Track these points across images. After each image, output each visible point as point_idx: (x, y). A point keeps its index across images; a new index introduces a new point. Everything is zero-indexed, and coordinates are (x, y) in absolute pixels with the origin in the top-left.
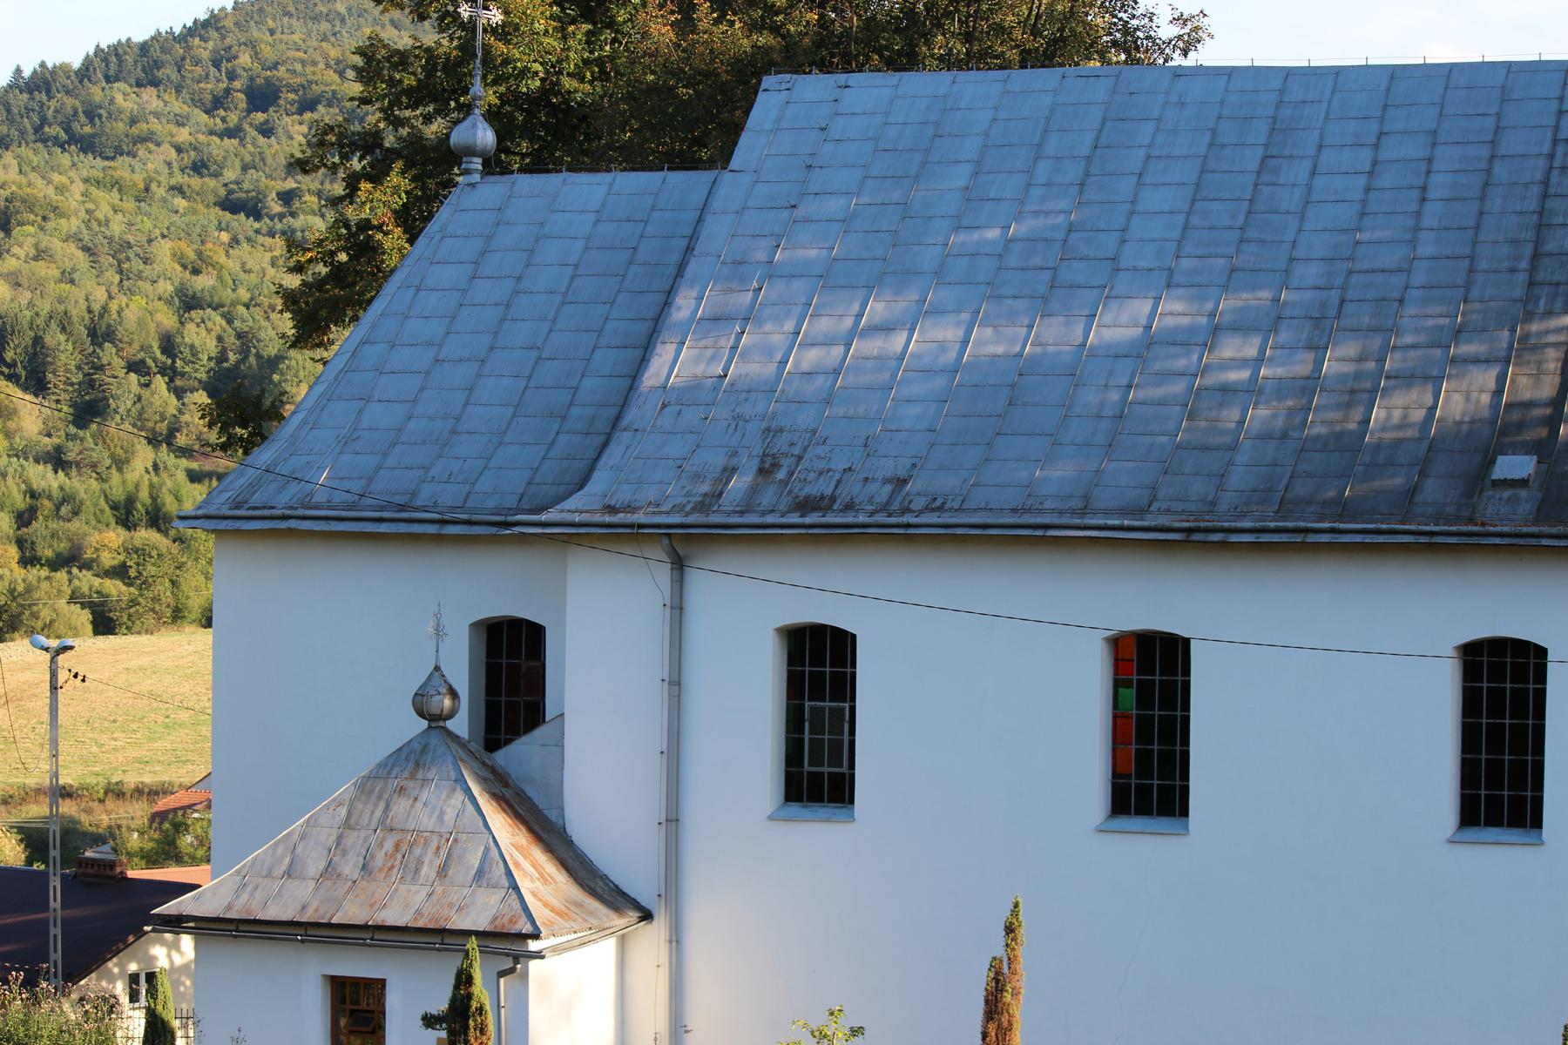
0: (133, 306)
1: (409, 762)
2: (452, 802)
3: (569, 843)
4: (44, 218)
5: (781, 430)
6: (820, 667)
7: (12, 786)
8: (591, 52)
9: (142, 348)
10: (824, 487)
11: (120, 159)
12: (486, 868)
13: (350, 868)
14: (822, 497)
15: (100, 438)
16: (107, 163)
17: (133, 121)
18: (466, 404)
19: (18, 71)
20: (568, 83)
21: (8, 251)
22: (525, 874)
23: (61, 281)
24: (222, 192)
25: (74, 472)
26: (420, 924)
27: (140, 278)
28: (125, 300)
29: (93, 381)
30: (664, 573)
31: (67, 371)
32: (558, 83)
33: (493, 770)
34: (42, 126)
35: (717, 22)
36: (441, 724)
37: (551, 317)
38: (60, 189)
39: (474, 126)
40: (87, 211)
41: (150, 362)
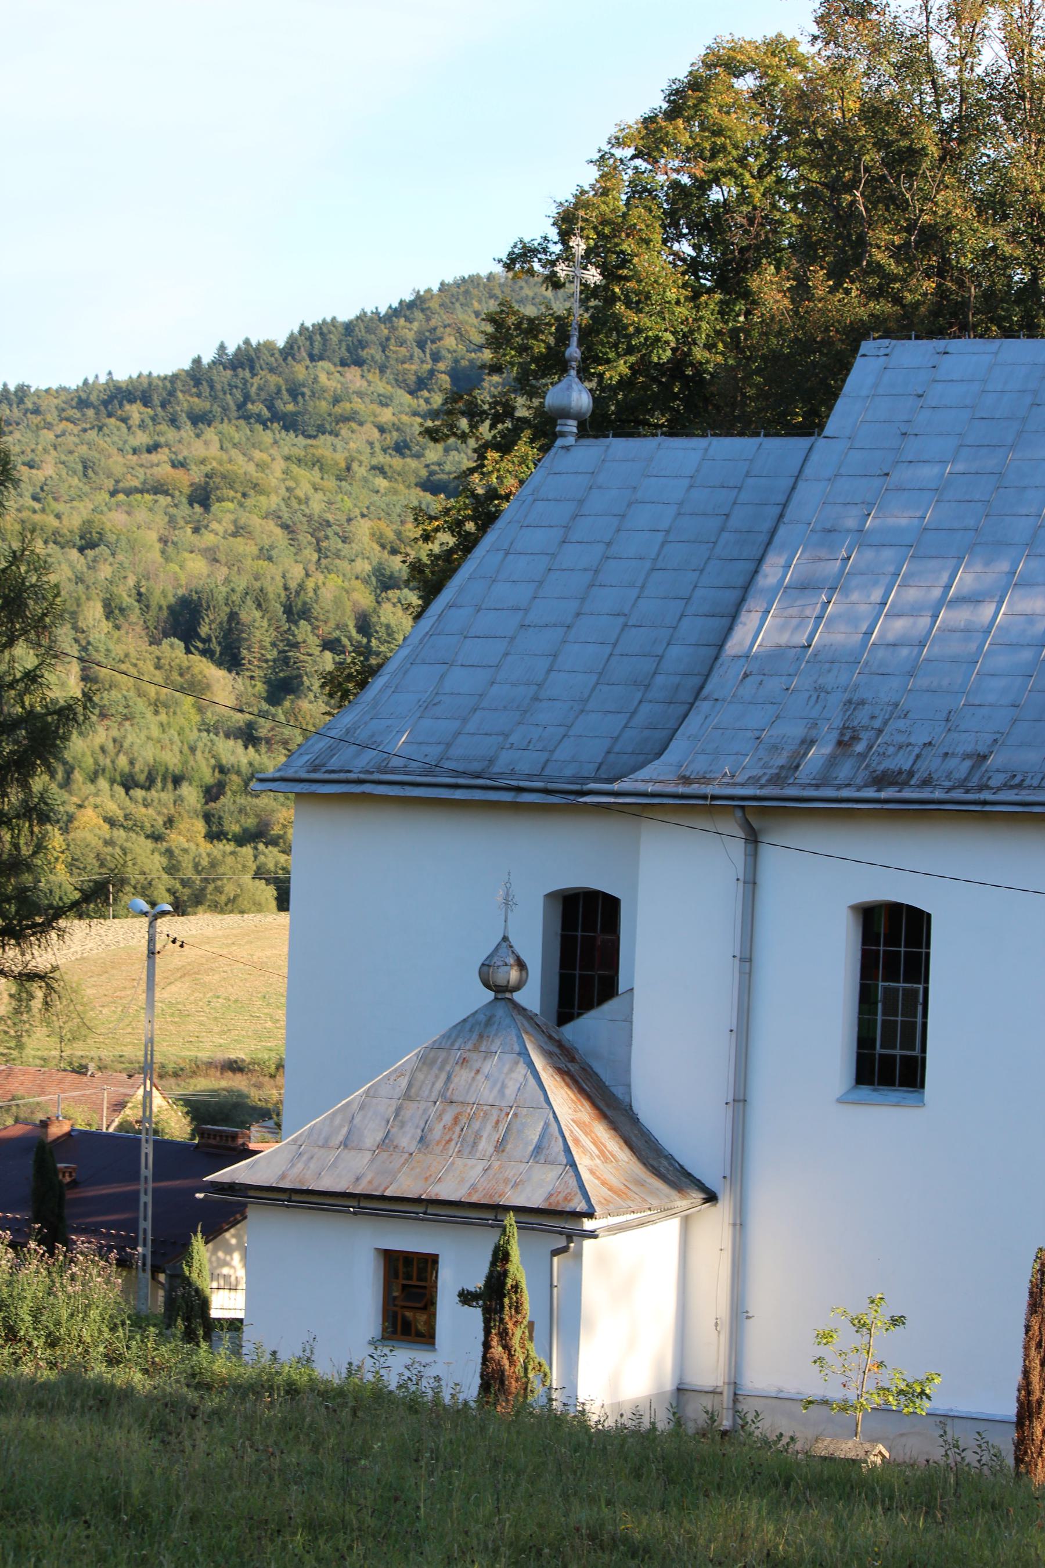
0: (330, 584)
1: (475, 1030)
2: (514, 1075)
3: (635, 1120)
4: (244, 495)
5: (862, 703)
6: (894, 945)
7: (184, 1059)
8: (726, 322)
9: (337, 627)
10: (903, 762)
11: (322, 438)
12: (545, 1144)
13: (407, 1140)
14: (900, 772)
15: (293, 714)
16: (309, 442)
17: (336, 401)
18: (550, 670)
19: (222, 347)
20: (699, 354)
21: (206, 527)
22: (585, 1151)
23: (259, 558)
24: (424, 473)
25: (263, 748)
26: (474, 1199)
27: (338, 557)
28: (321, 577)
29: (288, 658)
30: (737, 848)
31: (262, 647)
32: (689, 354)
33: (560, 1044)
34: (244, 403)
35: (832, 290)
36: (508, 995)
37: (639, 583)
38: (261, 466)
39: (569, 388)
40: (288, 489)
41: (345, 641)
